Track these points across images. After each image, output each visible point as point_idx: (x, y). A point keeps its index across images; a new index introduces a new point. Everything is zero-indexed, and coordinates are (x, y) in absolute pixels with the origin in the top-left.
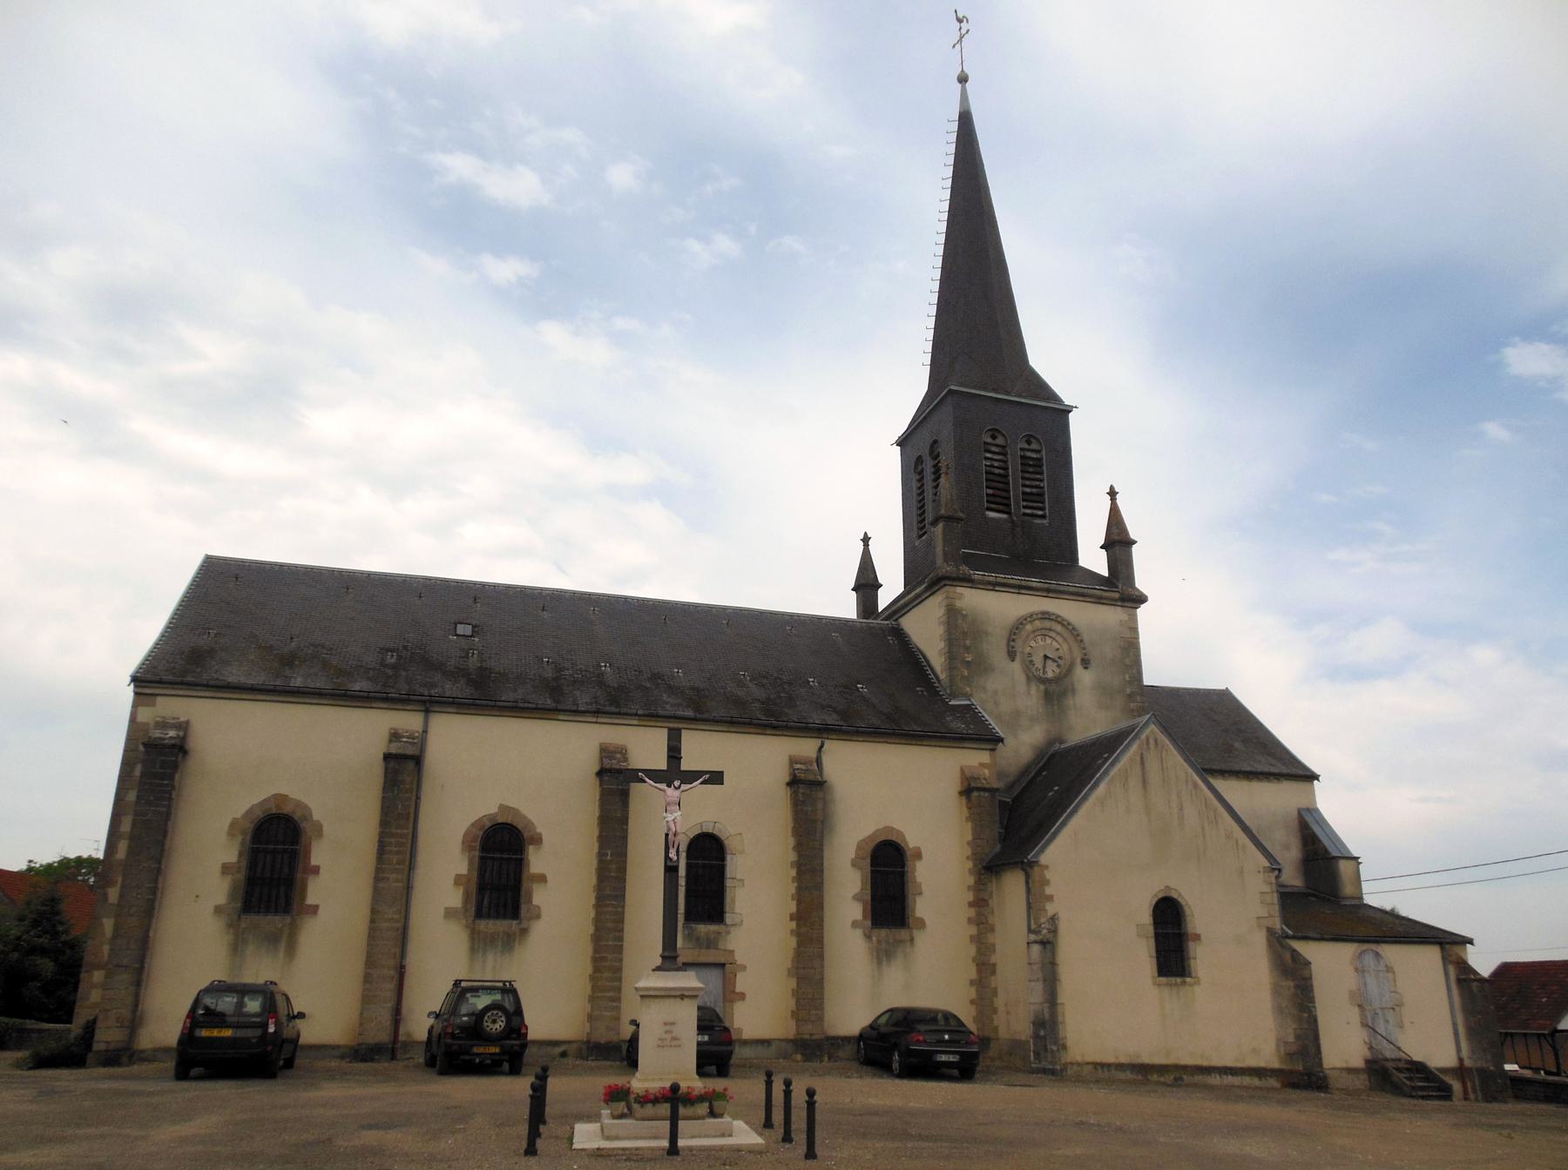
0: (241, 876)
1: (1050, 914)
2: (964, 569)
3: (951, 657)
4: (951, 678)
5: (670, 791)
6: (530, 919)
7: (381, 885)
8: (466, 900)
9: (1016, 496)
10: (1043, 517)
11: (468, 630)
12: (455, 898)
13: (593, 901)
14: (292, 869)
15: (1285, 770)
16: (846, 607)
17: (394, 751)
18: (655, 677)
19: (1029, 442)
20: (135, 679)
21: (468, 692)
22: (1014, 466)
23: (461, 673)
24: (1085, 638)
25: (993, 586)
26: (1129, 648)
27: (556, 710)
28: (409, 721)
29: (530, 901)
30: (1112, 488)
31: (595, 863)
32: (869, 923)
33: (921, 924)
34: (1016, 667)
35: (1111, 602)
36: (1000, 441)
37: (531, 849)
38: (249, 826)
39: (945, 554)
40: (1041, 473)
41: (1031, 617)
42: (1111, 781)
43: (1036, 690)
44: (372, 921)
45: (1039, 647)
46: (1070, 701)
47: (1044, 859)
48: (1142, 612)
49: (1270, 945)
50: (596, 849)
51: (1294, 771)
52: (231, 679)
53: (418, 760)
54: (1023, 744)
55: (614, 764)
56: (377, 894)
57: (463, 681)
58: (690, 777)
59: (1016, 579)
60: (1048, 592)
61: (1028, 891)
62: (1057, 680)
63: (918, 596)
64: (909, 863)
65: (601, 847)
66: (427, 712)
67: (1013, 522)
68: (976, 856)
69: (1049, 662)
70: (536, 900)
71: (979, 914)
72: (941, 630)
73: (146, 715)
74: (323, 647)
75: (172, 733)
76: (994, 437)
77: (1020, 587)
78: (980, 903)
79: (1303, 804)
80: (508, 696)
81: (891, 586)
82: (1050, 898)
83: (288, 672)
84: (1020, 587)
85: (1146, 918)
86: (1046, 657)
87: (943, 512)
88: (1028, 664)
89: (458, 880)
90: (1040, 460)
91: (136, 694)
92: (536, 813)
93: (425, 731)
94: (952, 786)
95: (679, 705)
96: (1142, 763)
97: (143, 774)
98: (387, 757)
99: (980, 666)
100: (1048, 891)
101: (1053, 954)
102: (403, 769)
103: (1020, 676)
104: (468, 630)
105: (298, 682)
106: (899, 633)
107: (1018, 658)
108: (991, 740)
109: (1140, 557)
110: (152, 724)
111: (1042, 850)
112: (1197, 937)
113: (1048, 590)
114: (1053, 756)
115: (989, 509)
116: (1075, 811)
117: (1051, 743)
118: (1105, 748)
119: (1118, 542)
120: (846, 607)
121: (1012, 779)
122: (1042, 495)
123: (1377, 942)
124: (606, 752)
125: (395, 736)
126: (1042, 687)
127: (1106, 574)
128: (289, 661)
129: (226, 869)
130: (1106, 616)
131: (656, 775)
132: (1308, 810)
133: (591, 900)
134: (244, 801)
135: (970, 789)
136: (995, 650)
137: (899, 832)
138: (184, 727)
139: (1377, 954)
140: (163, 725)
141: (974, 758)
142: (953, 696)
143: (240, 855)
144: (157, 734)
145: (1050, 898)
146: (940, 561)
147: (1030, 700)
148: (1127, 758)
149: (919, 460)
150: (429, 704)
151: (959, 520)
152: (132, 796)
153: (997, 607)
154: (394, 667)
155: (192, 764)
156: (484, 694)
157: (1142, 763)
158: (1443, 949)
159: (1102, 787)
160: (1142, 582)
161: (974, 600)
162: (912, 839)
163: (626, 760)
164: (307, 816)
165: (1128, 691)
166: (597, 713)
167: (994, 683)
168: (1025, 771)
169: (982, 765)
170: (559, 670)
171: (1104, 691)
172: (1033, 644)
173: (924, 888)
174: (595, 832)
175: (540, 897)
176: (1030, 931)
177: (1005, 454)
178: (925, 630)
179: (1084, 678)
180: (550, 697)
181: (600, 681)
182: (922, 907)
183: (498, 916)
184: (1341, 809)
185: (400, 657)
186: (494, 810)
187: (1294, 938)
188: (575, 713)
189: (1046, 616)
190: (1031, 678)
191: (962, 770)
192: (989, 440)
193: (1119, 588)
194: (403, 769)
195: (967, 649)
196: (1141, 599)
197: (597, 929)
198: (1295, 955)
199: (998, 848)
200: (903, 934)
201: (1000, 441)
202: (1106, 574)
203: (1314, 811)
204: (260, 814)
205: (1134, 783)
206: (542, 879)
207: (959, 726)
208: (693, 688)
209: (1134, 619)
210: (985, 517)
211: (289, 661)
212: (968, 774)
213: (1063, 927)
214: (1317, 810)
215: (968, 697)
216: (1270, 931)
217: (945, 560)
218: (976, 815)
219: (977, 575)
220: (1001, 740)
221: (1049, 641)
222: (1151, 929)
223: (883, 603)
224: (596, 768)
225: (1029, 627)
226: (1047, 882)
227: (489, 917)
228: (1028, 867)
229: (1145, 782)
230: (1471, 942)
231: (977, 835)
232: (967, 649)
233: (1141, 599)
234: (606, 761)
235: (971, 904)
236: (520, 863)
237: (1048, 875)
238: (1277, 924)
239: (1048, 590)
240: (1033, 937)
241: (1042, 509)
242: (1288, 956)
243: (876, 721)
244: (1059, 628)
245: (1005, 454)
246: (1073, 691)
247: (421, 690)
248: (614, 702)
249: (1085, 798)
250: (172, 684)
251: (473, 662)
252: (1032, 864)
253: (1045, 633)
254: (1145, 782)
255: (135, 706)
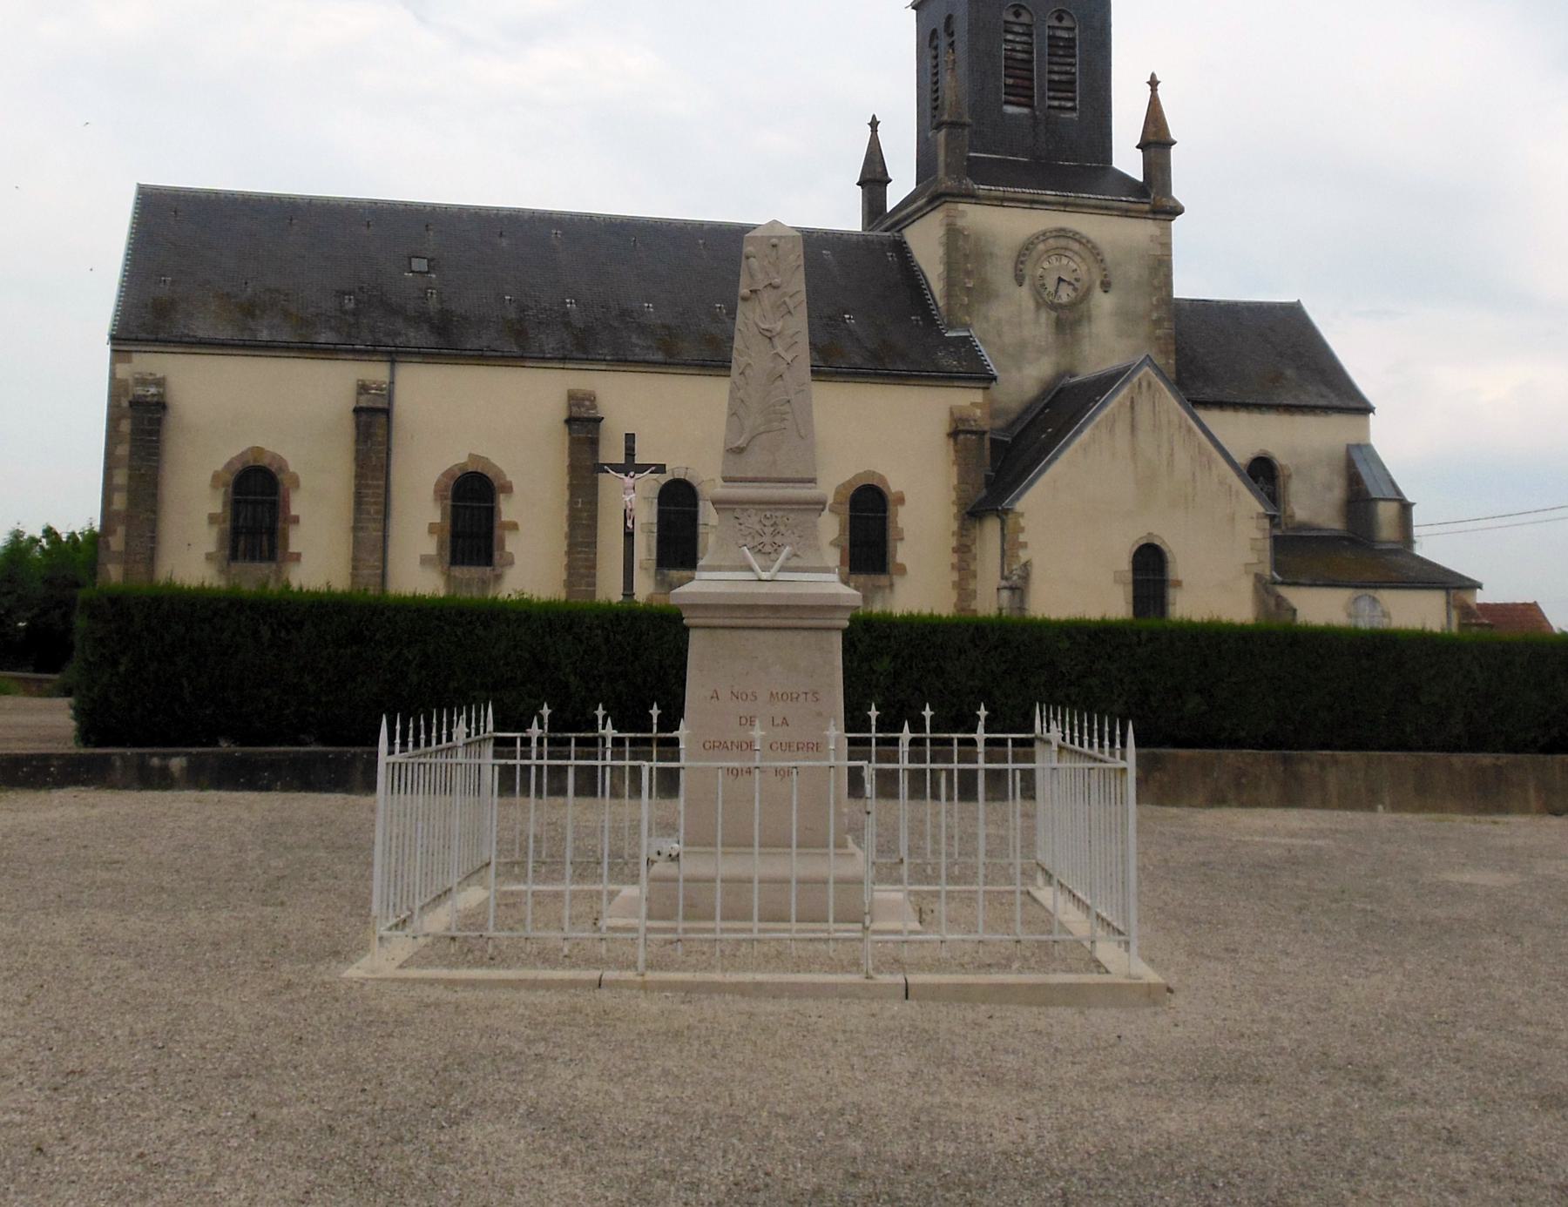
0: (227, 525)
1: (1023, 560)
2: (968, 183)
3: (950, 283)
4: (949, 310)
5: (627, 479)
6: (503, 566)
7: (361, 534)
8: (441, 546)
9: (1041, 87)
10: (1073, 109)
11: (420, 265)
12: (430, 546)
13: (565, 548)
14: (274, 519)
15: (1336, 402)
16: (843, 214)
17: (363, 404)
18: (624, 313)
19: (1060, 19)
20: (114, 339)
21: (432, 340)
22: (1040, 47)
23: (422, 318)
24: (1108, 257)
25: (1001, 202)
26: (1161, 267)
27: (522, 358)
28: (376, 372)
29: (503, 548)
30: (1153, 76)
31: (566, 512)
32: (847, 569)
33: (902, 570)
34: (1024, 294)
35: (1140, 215)
36: (1025, 18)
37: (502, 496)
38: (230, 478)
39: (947, 165)
40: (1074, 56)
41: (1044, 236)
42: (1097, 427)
43: (1046, 317)
44: (354, 568)
45: (1052, 268)
46: (1084, 330)
47: (1019, 506)
48: (1177, 224)
49: (1256, 590)
50: (567, 497)
51: (1353, 404)
52: (201, 334)
53: (387, 412)
54: (1023, 378)
55: (583, 412)
56: (357, 544)
57: (426, 327)
58: (642, 468)
59: (1028, 193)
60: (1065, 206)
61: (1003, 536)
62: (1072, 306)
63: (920, 209)
64: (891, 507)
65: (572, 495)
66: (393, 362)
67: (1034, 117)
68: (961, 502)
69: (1063, 286)
70: (509, 548)
71: (961, 560)
72: (941, 251)
73: (124, 371)
74: (277, 291)
75: (153, 390)
76: (1017, 15)
77: (1033, 202)
78: (964, 550)
79: (1353, 439)
80: (472, 343)
81: (902, 184)
82: (1024, 545)
83: (251, 324)
84: (1033, 202)
85: (1125, 565)
86: (1060, 280)
87: (946, 118)
88: (1038, 290)
89: (432, 529)
90: (1073, 39)
91: (113, 351)
92: (505, 461)
93: (392, 383)
94: (942, 426)
95: (649, 347)
96: (1132, 408)
97: (133, 432)
98: (358, 411)
99: (983, 293)
100: (1022, 538)
101: (1022, 600)
102: (373, 421)
103: (1030, 304)
104: (420, 265)
105: (264, 335)
106: (901, 248)
107: (1027, 282)
108: (982, 377)
109: (1178, 157)
110: (131, 382)
111: (1017, 498)
112: (1178, 584)
113: (1065, 204)
114: (1061, 391)
115: (1008, 103)
116: (1055, 458)
117: (1060, 376)
118: (1104, 384)
119: (1156, 142)
120: (843, 214)
121: (1013, 416)
122: (1072, 83)
123: (1376, 588)
124: (575, 399)
125: (363, 388)
126: (1054, 314)
127: (1141, 179)
128: (250, 310)
129: (213, 519)
130: (1138, 231)
131: (617, 468)
132: (1358, 446)
133: (563, 546)
134: (224, 454)
135: (959, 431)
136: (1000, 274)
137: (882, 478)
138: (160, 383)
139: (1374, 599)
140: (143, 382)
141: (966, 398)
142: (951, 327)
143: (225, 505)
144: (140, 391)
145: (1024, 545)
146: (941, 173)
147: (1038, 328)
148: (1116, 402)
149: (934, 32)
150: (394, 355)
151: (963, 125)
152: (123, 450)
153: (1004, 224)
154: (355, 313)
155: (171, 420)
156: (449, 340)
157: (1132, 408)
158: (1448, 594)
159: (1086, 434)
160: (1179, 191)
161: (975, 216)
162: (895, 484)
163: (594, 407)
164: (283, 466)
165: (1155, 316)
166: (564, 359)
167: (998, 311)
168: (1028, 408)
169: (974, 404)
170: (522, 309)
171: (1125, 316)
172: (1046, 265)
173: (906, 534)
174: (565, 480)
175: (512, 544)
176: (1003, 578)
177: (1030, 35)
178: (926, 244)
179: (1103, 304)
180: (515, 341)
181: (565, 320)
182: (902, 553)
183: (471, 563)
184: (1398, 441)
185: (358, 302)
186: (463, 459)
187: (1282, 583)
188: (542, 359)
189: (1061, 233)
190: (1041, 303)
191: (952, 413)
192: (1012, 18)
193: (1152, 198)
194: (373, 421)
195: (968, 273)
196: (1177, 211)
197: (570, 575)
198: (1280, 600)
199: (984, 492)
200: (883, 580)
201: (1025, 18)
202: (1141, 179)
203: (1365, 449)
204: (239, 466)
205: (1122, 428)
206: (514, 526)
207: (949, 362)
208: (664, 326)
209: (1168, 233)
210: (1003, 115)
211: (250, 310)
212: (957, 415)
213: (1036, 574)
214: (1369, 447)
215: (967, 327)
216: (1258, 578)
217: (947, 174)
218: (963, 460)
219: (982, 189)
220: (994, 378)
221: (1064, 261)
222: (1130, 575)
223: (891, 204)
224: (564, 415)
225: (1041, 247)
226: (1022, 530)
227: (463, 564)
228: (1003, 514)
229: (1133, 428)
230: (1480, 586)
231: (962, 479)
232: (968, 273)
233: (1177, 211)
234: (575, 409)
235: (955, 550)
236: (490, 513)
237: (1022, 522)
238: (1267, 570)
239: (1065, 204)
240: (1004, 583)
241: (1073, 100)
242: (1272, 602)
243: (858, 360)
244: (1076, 246)
245: (1030, 35)
246: (1089, 318)
247: (386, 340)
248: (581, 346)
249: (1067, 444)
250: (147, 341)
251: (433, 304)
252: (1006, 512)
253: (1060, 252)
254: (1133, 428)
255: (113, 363)
